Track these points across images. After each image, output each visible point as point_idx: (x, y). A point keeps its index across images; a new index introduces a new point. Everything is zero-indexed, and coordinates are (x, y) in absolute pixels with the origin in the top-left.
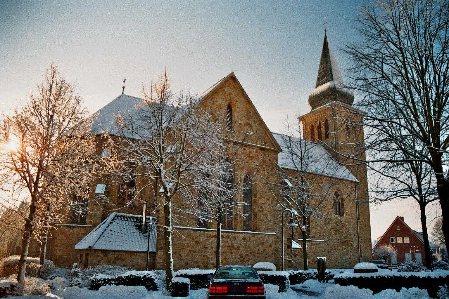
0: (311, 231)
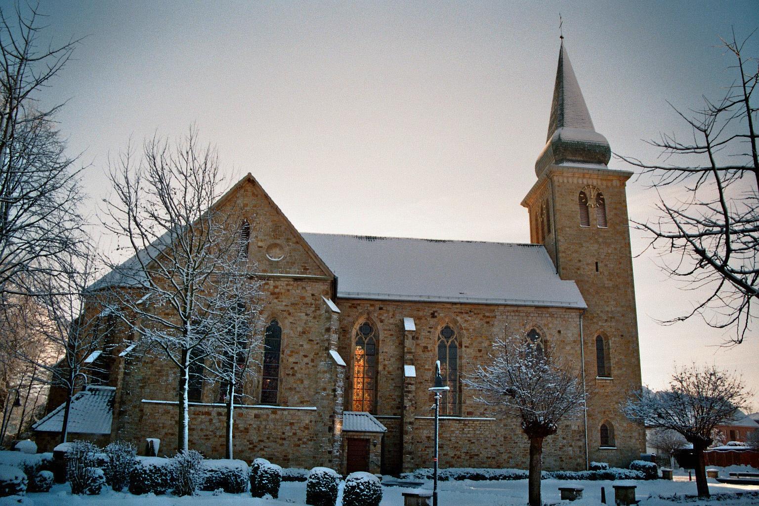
0: (465, 403)
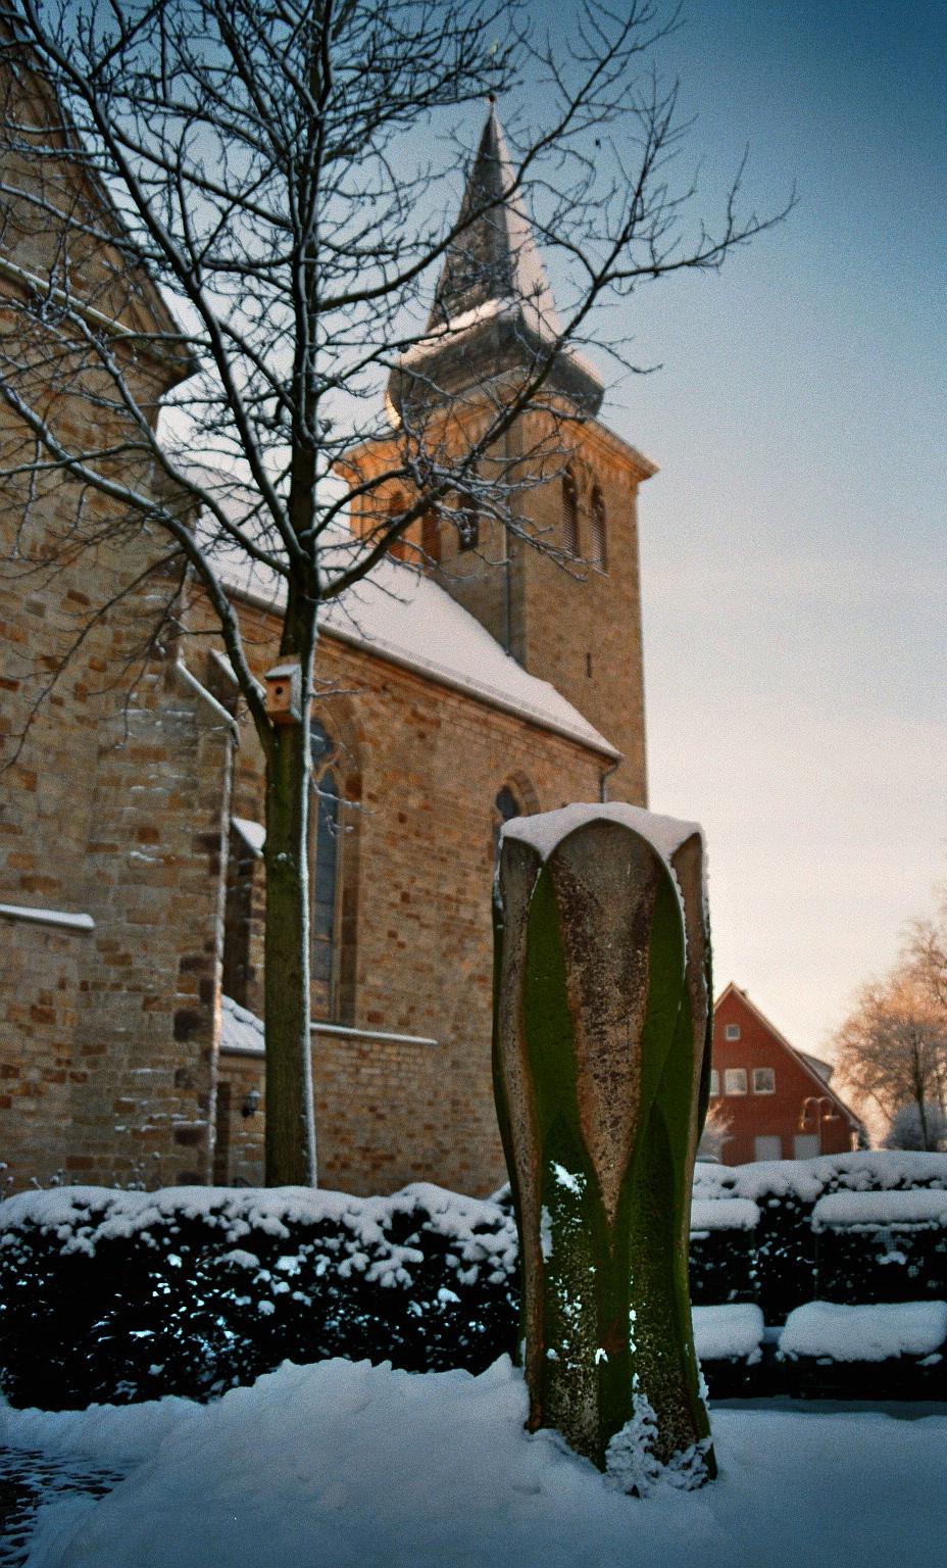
0: (363, 980)
